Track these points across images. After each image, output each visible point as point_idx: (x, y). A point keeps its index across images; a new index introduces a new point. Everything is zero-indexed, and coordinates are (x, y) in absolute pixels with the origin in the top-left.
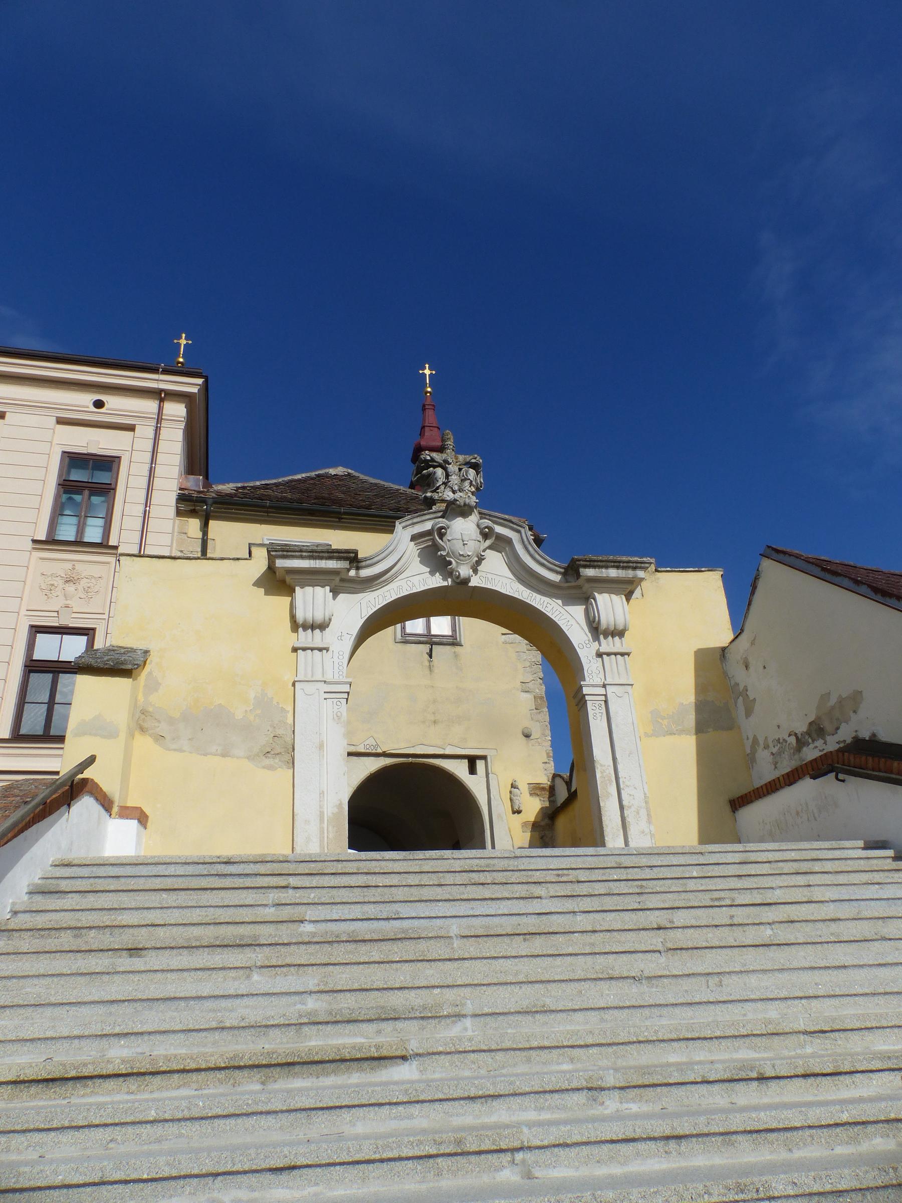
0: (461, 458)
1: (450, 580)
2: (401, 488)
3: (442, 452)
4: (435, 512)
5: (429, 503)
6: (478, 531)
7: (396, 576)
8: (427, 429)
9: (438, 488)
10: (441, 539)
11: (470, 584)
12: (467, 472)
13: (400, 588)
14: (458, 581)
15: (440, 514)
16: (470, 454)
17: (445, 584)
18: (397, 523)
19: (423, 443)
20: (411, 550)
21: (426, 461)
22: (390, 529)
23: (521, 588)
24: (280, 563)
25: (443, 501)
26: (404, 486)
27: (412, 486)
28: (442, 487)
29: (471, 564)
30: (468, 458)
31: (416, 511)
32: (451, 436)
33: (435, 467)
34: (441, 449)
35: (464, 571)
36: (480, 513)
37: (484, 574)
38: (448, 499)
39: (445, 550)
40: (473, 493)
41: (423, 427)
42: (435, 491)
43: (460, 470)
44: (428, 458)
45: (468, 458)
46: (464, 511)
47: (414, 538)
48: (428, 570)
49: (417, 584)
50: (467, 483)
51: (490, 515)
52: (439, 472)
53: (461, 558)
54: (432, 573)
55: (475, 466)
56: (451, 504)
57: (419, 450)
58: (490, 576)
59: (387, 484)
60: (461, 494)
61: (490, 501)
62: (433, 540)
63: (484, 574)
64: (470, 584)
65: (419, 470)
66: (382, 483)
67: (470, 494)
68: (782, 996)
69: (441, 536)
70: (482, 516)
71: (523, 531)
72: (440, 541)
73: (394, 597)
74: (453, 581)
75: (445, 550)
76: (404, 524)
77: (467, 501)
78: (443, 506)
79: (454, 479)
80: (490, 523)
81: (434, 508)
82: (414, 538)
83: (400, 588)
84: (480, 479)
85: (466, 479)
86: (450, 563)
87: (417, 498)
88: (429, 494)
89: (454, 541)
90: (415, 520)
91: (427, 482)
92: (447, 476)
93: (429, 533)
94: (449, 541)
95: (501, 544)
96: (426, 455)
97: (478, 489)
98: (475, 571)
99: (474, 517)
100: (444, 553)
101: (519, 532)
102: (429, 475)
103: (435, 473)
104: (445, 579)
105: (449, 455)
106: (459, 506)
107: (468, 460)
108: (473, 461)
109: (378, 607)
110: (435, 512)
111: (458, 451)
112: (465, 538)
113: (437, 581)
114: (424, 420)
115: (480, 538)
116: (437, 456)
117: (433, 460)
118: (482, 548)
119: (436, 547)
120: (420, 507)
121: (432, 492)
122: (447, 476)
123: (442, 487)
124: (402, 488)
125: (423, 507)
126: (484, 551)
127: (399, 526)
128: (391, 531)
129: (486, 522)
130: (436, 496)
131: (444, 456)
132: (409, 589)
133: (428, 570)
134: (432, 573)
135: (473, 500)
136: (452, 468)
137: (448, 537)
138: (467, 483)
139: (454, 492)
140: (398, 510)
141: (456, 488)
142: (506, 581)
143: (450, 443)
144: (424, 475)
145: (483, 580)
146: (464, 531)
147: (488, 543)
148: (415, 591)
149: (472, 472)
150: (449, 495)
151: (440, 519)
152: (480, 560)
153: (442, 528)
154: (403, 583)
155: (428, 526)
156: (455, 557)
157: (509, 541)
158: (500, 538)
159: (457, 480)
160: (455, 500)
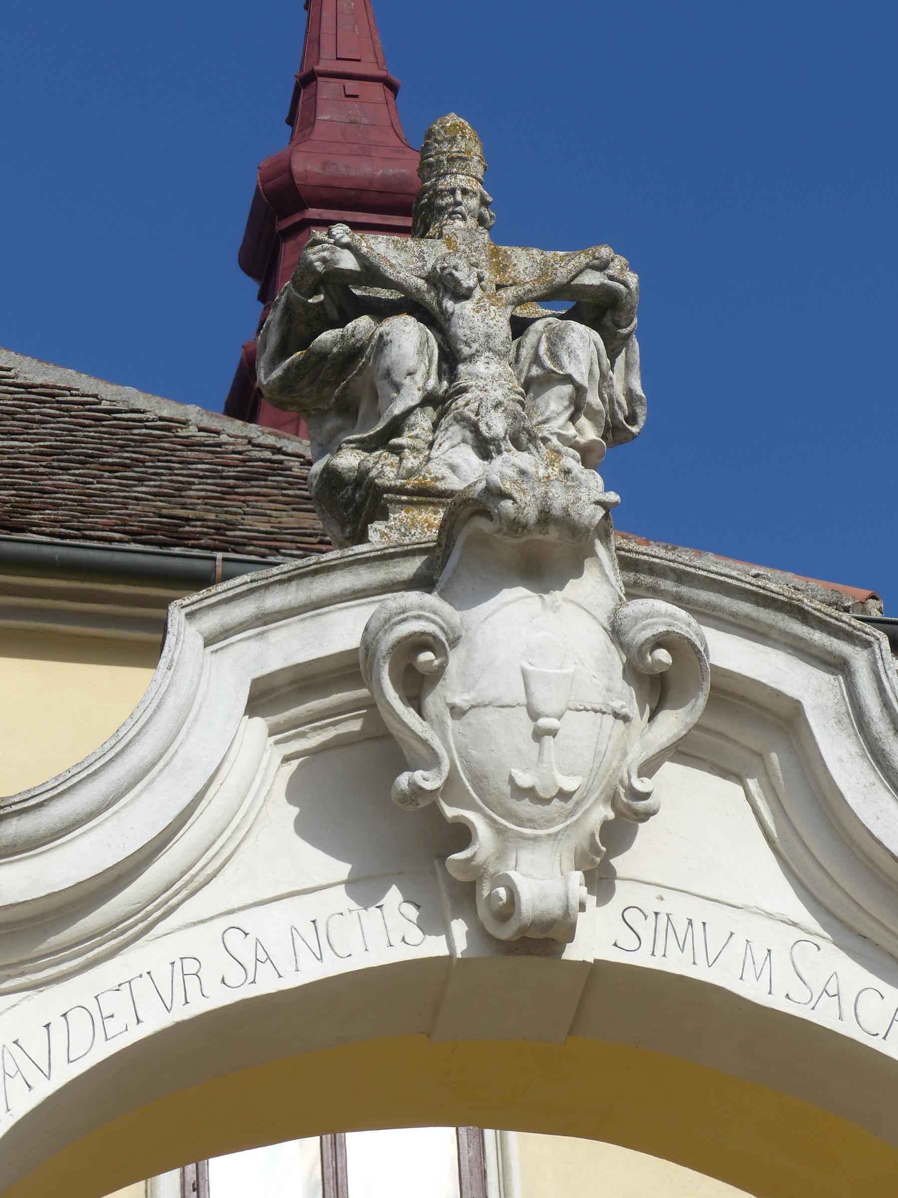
0: (525, 263)
1: (459, 928)
2: (192, 412)
3: (419, 231)
4: (384, 558)
5: (353, 506)
6: (617, 660)
7: (190, 884)
8: (327, 89)
9: (397, 426)
10: (415, 701)
11: (573, 952)
12: (555, 340)
13: (186, 968)
14: (506, 932)
15: (410, 568)
16: (574, 244)
17: (434, 947)
18: (176, 615)
19: (307, 166)
20: (256, 762)
21: (333, 280)
22: (143, 646)
23: (853, 975)
24: (363, 692)
25: (426, 495)
26: (206, 406)
27: (244, 402)
28: (423, 420)
29: (578, 840)
30: (565, 265)
31: (271, 546)
32: (469, 144)
33: (381, 311)
34: (412, 209)
35: (540, 879)
36: (627, 564)
37: (647, 898)
38: (454, 483)
39: (432, 761)
40: (586, 454)
41: (307, 80)
42: (385, 440)
43: (519, 327)
44: (348, 262)
45: (565, 265)
46: (540, 554)
47: (264, 697)
48: (342, 870)
49: (264, 958)
50: (555, 401)
51: (681, 577)
52: (407, 337)
53: (525, 807)
54: (364, 888)
55: (598, 310)
56: (471, 511)
57: (280, 213)
58: (679, 908)
59: (110, 393)
60: (523, 459)
61: (676, 490)
62: (372, 708)
63: (647, 898)
64: (573, 952)
65: (298, 330)
66: (86, 384)
67: (572, 461)
68: (595, 613)
69: (417, 685)
70: (639, 576)
71: (859, 659)
72: (409, 715)
73: (156, 1021)
74: (478, 932)
75: (432, 761)
76: (212, 621)
77: (559, 498)
78: (426, 524)
79: (489, 379)
80: (681, 621)
81: (379, 535)
82: (264, 697)
83: (186, 968)
84: (627, 379)
85: (550, 379)
86: (463, 835)
87: (277, 468)
88: (348, 460)
89: (489, 717)
90: (275, 600)
91: (341, 390)
92: (450, 359)
93: (348, 670)
94: (457, 712)
95: (742, 732)
96: (337, 247)
97: (613, 431)
98: (601, 880)
99: (596, 586)
100: (428, 780)
101: (838, 666)
102: (352, 355)
103: (382, 343)
104: (433, 922)
105: (459, 245)
106: (516, 526)
107: (561, 275)
108: (592, 279)
109: (65, 1074)
110: (384, 558)
111: (508, 225)
112: (545, 700)
113: (390, 934)
114: (312, 41)
115: (626, 698)
116: (399, 258)
117: (371, 273)
118: (638, 754)
119: (384, 749)
120: (290, 519)
121: (368, 446)
122: (450, 359)
123: (423, 420)
124: (195, 416)
125: (312, 521)
126: (648, 769)
127: (184, 631)
128: (147, 651)
129: (659, 614)
130: (386, 469)
131: (433, 252)
132: (235, 975)
133: (342, 870)
134: (364, 888)
135: (588, 494)
136: (478, 319)
137: (452, 690)
138: (555, 401)
139: (485, 448)
140: (173, 534)
141: (497, 425)
142: (767, 934)
143: (465, 181)
144: (323, 356)
145: (645, 928)
146: (539, 658)
147: (672, 724)
148: (268, 984)
149: (582, 343)
150: (457, 465)
151: (413, 597)
152: (620, 830)
153: (420, 643)
154: (203, 942)
155: (341, 631)
156: (490, 802)
157: (784, 719)
158: (734, 697)
159: (500, 373)
160: (495, 493)
